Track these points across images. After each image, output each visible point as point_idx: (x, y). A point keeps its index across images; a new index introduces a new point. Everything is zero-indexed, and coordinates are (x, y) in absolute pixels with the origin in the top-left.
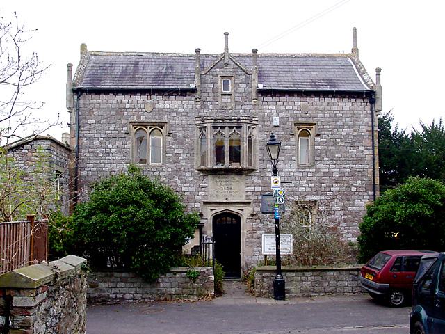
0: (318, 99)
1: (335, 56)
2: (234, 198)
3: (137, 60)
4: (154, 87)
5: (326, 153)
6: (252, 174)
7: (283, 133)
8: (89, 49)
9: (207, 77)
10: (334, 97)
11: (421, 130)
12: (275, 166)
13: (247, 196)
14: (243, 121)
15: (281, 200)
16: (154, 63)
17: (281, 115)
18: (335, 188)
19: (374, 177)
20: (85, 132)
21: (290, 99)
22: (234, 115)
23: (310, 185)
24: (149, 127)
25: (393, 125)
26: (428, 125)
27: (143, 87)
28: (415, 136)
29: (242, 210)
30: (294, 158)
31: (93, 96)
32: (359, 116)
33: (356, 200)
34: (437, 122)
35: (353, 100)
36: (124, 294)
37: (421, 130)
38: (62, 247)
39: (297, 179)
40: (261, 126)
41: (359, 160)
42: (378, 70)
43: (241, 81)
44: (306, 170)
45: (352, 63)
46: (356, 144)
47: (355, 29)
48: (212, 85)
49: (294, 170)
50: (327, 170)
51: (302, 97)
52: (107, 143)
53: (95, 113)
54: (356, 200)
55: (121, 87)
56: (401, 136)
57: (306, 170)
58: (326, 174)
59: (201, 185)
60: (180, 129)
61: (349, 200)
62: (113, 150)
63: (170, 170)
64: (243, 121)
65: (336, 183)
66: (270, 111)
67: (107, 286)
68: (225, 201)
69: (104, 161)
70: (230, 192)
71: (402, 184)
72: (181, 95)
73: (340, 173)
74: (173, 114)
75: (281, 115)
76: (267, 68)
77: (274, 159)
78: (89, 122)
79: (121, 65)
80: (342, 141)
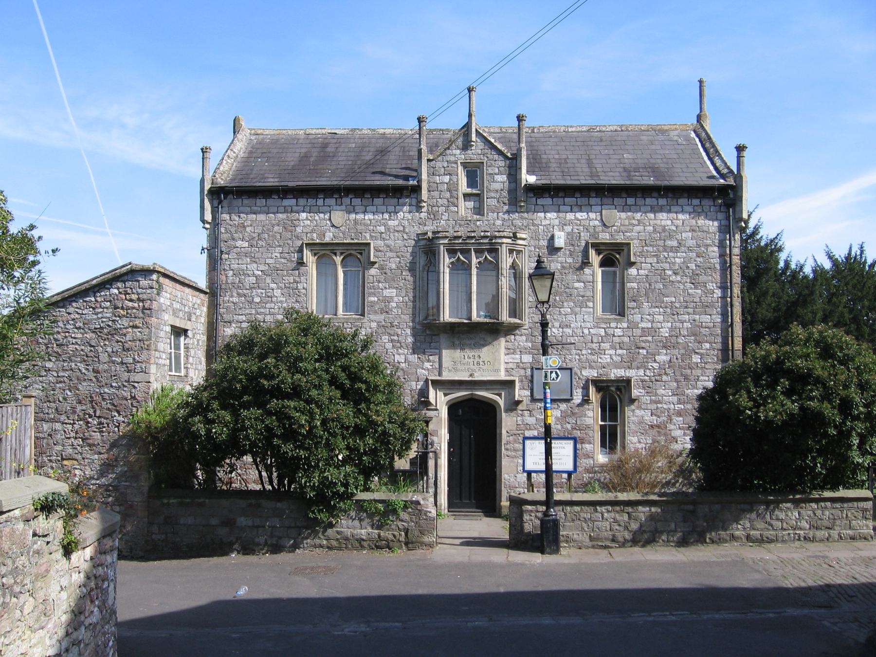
0: (633, 200)
1: (666, 128)
2: (484, 373)
3: (326, 141)
4: (347, 183)
5: (646, 294)
9: (439, 164)
10: (662, 197)
11: (827, 265)
12: (543, 315)
13: (507, 370)
15: (554, 375)
16: (354, 145)
17: (568, 229)
18: (662, 358)
20: (231, 262)
21: (583, 201)
22: (483, 229)
23: (620, 352)
24: (338, 253)
25: (783, 256)
26: (840, 254)
27: (329, 183)
28: (818, 271)
30: (591, 304)
31: (246, 201)
32: (705, 229)
33: (701, 378)
34: (855, 250)
35: (696, 202)
36: (280, 538)
37: (827, 265)
38: (782, 380)
39: (595, 340)
41: (705, 307)
42: (740, 149)
45: (697, 140)
46: (703, 278)
47: (701, 82)
48: (447, 179)
50: (650, 326)
51: (605, 196)
52: (268, 280)
53: (248, 229)
54: (701, 378)
55: (291, 184)
56: (795, 274)
58: (645, 332)
61: (686, 378)
62: (278, 293)
63: (374, 325)
65: (665, 347)
66: (548, 222)
67: (250, 523)
69: (262, 310)
71: (548, 326)
72: (394, 197)
73: (671, 329)
75: (568, 229)
76: (551, 154)
77: (543, 303)
78: (239, 243)
79: (298, 150)
80: (676, 274)
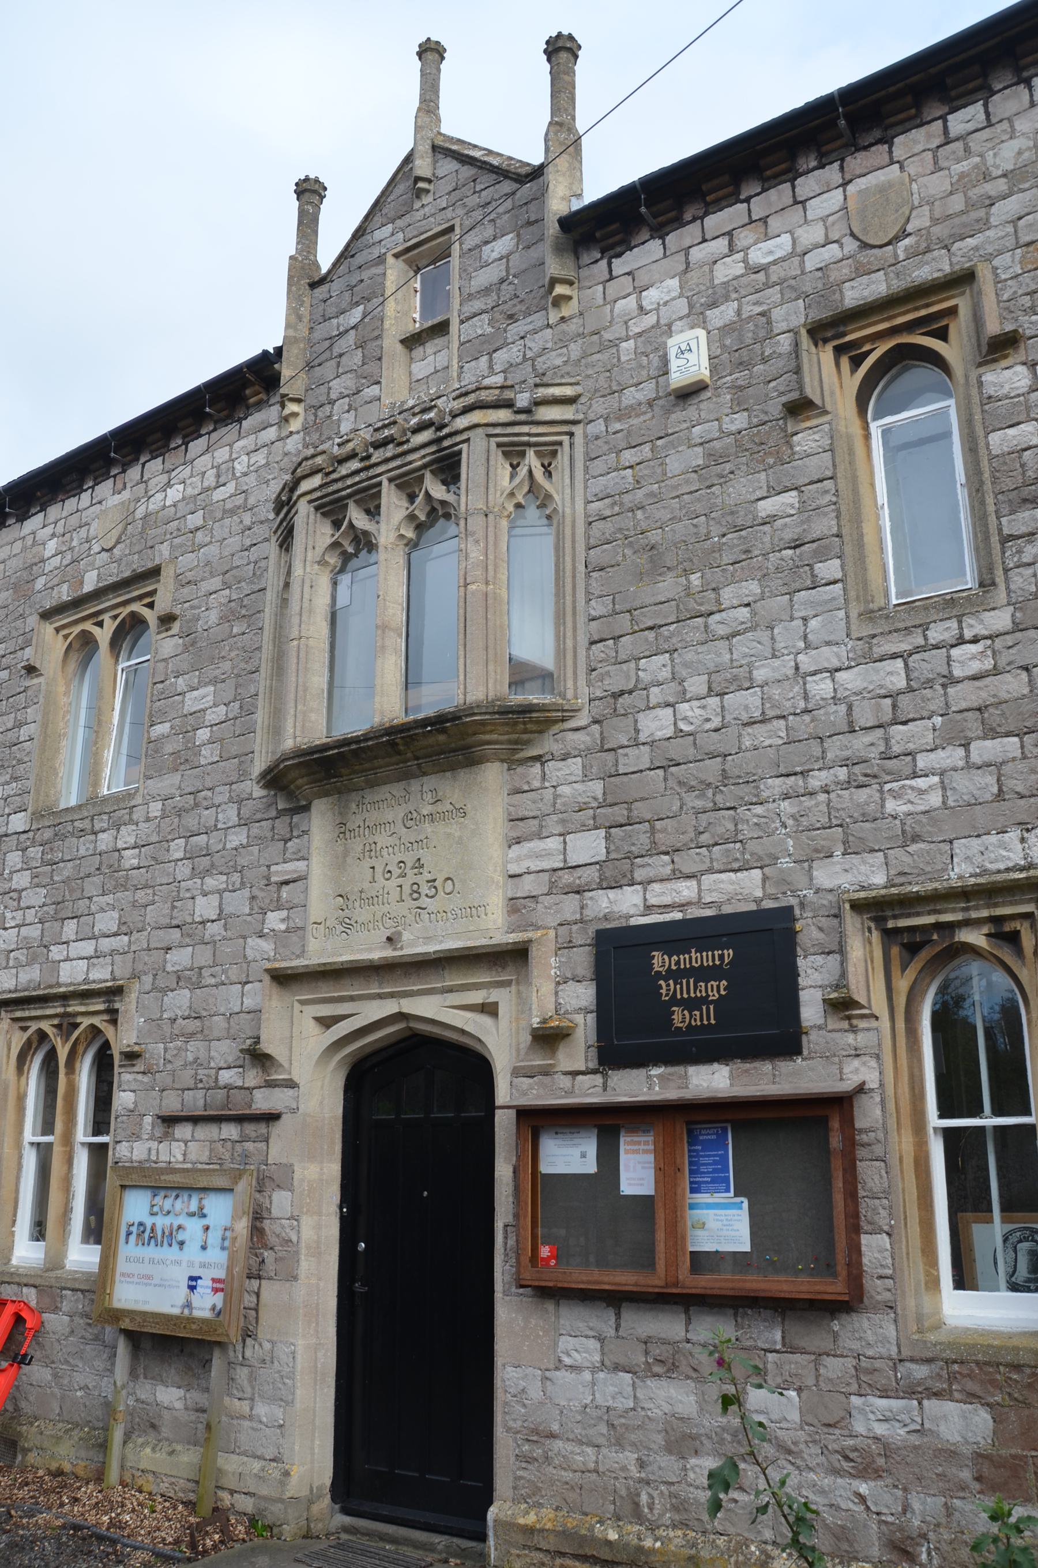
6: (548, 744)
7: (740, 421)
8: (442, 521)
14: (461, 422)
19: (465, 684)
23: (984, 749)
29: (489, 1009)
30: (829, 569)
39: (864, 716)
40: (599, 427)
43: (923, 761)
44: (935, 634)
49: (829, 657)
57: (935, 634)
59: (283, 870)
60: (216, 583)
64: (461, 422)
68: (378, 954)
70: (416, 892)
74: (195, 520)
